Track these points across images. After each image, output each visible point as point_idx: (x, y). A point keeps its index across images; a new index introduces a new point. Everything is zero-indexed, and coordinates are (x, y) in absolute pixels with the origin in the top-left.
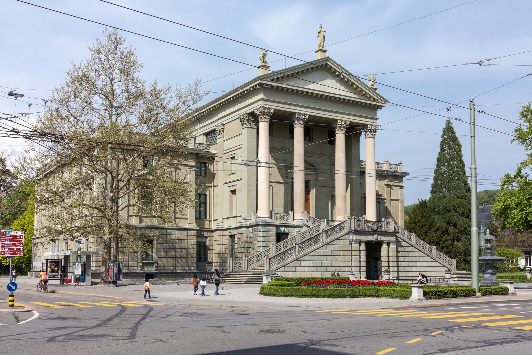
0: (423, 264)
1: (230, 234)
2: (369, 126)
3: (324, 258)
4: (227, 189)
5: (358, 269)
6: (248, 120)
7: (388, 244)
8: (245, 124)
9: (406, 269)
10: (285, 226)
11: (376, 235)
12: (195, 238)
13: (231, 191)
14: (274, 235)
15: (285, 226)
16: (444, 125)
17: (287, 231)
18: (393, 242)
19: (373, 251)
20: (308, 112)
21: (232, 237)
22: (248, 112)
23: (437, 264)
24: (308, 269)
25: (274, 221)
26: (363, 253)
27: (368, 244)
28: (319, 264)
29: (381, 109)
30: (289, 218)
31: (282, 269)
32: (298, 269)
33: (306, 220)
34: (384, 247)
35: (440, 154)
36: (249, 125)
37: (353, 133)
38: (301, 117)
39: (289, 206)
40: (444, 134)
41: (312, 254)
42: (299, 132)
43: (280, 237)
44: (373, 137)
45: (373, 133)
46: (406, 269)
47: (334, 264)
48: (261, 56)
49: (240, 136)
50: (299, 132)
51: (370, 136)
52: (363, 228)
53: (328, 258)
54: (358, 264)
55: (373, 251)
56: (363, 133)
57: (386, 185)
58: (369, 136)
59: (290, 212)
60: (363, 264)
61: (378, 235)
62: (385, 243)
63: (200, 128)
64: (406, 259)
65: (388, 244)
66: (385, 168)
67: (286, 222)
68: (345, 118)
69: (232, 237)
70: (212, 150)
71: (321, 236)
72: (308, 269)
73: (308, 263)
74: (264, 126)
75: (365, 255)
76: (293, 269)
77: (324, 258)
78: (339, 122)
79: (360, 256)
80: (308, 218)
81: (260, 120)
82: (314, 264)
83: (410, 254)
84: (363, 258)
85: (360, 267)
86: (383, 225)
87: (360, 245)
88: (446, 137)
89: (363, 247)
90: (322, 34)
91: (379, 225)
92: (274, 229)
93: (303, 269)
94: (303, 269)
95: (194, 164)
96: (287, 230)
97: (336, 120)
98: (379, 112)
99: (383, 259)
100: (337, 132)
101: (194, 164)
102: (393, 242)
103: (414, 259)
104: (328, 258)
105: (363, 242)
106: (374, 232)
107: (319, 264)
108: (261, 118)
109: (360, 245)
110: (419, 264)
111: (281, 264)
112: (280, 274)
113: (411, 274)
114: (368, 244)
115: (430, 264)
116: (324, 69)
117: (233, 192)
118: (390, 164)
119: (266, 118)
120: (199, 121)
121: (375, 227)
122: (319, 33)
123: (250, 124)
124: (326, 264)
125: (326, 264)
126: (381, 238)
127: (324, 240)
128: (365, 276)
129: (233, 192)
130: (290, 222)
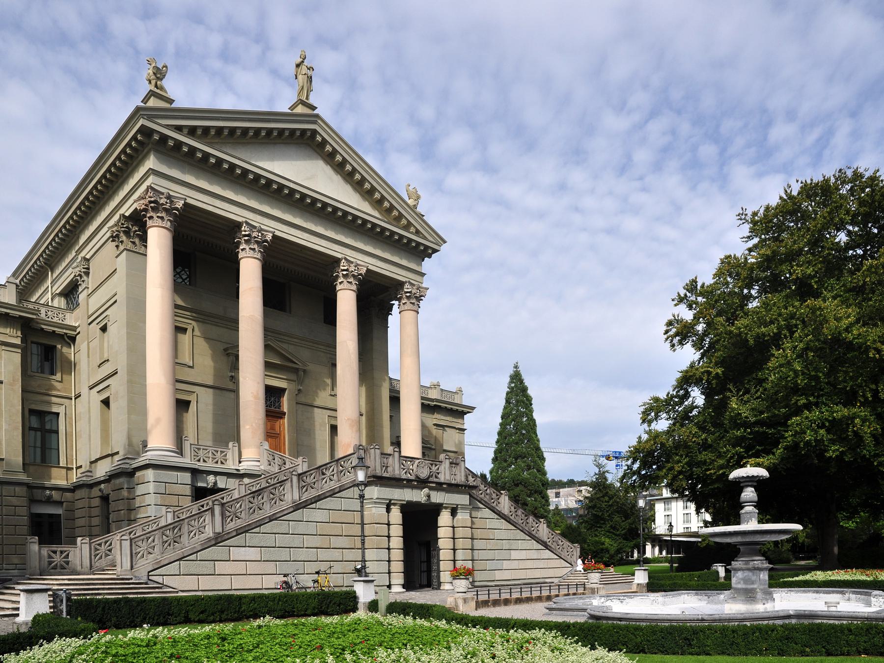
0: (523, 555)
1: (100, 494)
2: (406, 286)
3: (297, 541)
4: (96, 398)
5: (384, 567)
6: (127, 233)
7: (454, 512)
8: (122, 242)
9: (489, 565)
10: (216, 474)
11: (426, 490)
12: (24, 501)
13: (102, 401)
14: (188, 490)
15: (216, 474)
16: (511, 371)
17: (221, 485)
18: (464, 507)
19: (419, 525)
20: (272, 228)
21: (105, 499)
22: (127, 214)
23: (547, 554)
24: (252, 568)
25: (187, 461)
26: (397, 531)
27: (410, 511)
28: (284, 554)
29: (430, 256)
30: (229, 456)
31: (173, 568)
32: (220, 567)
33: (267, 463)
34: (444, 518)
35: (505, 408)
36: (130, 246)
37: (377, 298)
38: (255, 234)
39: (228, 431)
40: (511, 382)
41: (263, 529)
42: (250, 272)
43: (199, 494)
44: (415, 308)
45: (414, 301)
46: (489, 565)
47: (323, 555)
48: (151, 72)
49: (116, 276)
50: (250, 272)
51: (409, 306)
52: (397, 472)
53: (309, 541)
54: (384, 554)
55: (419, 525)
56: (395, 310)
57: (435, 425)
58: (406, 307)
59: (231, 444)
60: (398, 555)
61: (431, 489)
62: (446, 508)
63: (53, 282)
64: (490, 544)
65: (454, 512)
66: (433, 394)
67: (219, 465)
68: (358, 257)
69: (105, 499)
70: (71, 320)
71: (288, 485)
72: (252, 568)
73: (252, 553)
74: (159, 239)
75: (401, 546)
76: (207, 567)
77: (297, 541)
78: (343, 265)
79: (389, 537)
80: (271, 458)
81: (149, 223)
82: (267, 554)
83: (498, 534)
84: (397, 542)
85: (389, 561)
86: (442, 468)
87: (388, 510)
88: (513, 385)
89: (396, 515)
90: (304, 70)
91: (434, 468)
92: (187, 477)
93: (240, 568)
94: (240, 568)
95: (18, 341)
96: (222, 482)
97: (337, 261)
98: (427, 265)
99: (441, 543)
100: (338, 287)
101: (18, 341)
102: (464, 507)
103: (505, 545)
104: (309, 541)
105: (394, 504)
106: (421, 483)
107: (284, 554)
108: (151, 218)
109: (388, 510)
110: (514, 555)
111: (171, 555)
112: (167, 581)
113: (499, 575)
114: (410, 511)
115: (534, 554)
116: (309, 145)
117: (106, 402)
118: (442, 390)
119: (162, 218)
120: (50, 266)
121: (424, 473)
122: (298, 66)
123: (134, 243)
124: (302, 554)
125: (302, 554)
126: (437, 497)
127: (296, 497)
128: (402, 581)
129: (106, 402)
130: (231, 465)
